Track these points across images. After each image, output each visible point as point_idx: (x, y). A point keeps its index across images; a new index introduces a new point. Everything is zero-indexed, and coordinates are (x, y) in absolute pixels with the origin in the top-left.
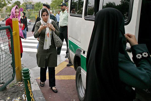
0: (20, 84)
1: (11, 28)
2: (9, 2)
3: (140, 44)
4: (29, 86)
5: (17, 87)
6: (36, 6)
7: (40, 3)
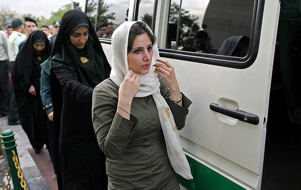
4: (15, 160)
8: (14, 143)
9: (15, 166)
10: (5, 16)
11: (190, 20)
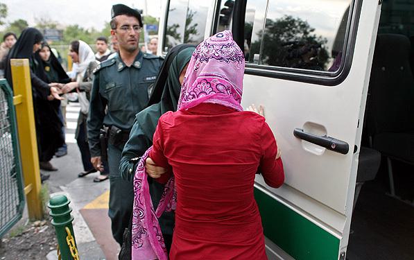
0: (39, 226)
1: (8, 86)
4: (71, 242)
5: (32, 236)
6: (68, 33)
7: (77, 26)
8: (68, 216)
9: (70, 253)
10: (45, 26)
11: (316, 42)
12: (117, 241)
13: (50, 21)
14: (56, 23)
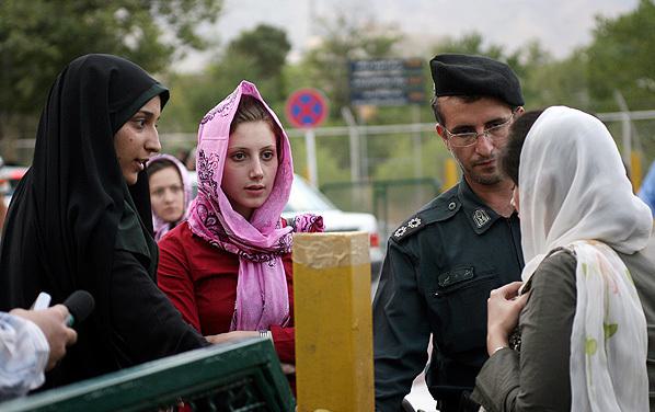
2: (187, 36)
3: (474, 403)
12: (519, 220)
13: (370, 26)
14: (391, 35)
